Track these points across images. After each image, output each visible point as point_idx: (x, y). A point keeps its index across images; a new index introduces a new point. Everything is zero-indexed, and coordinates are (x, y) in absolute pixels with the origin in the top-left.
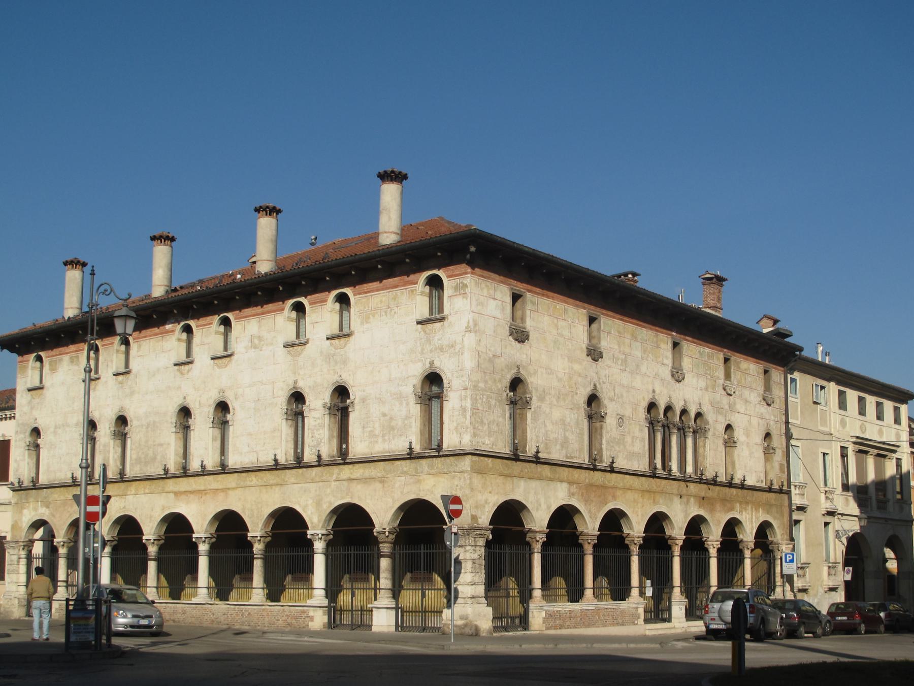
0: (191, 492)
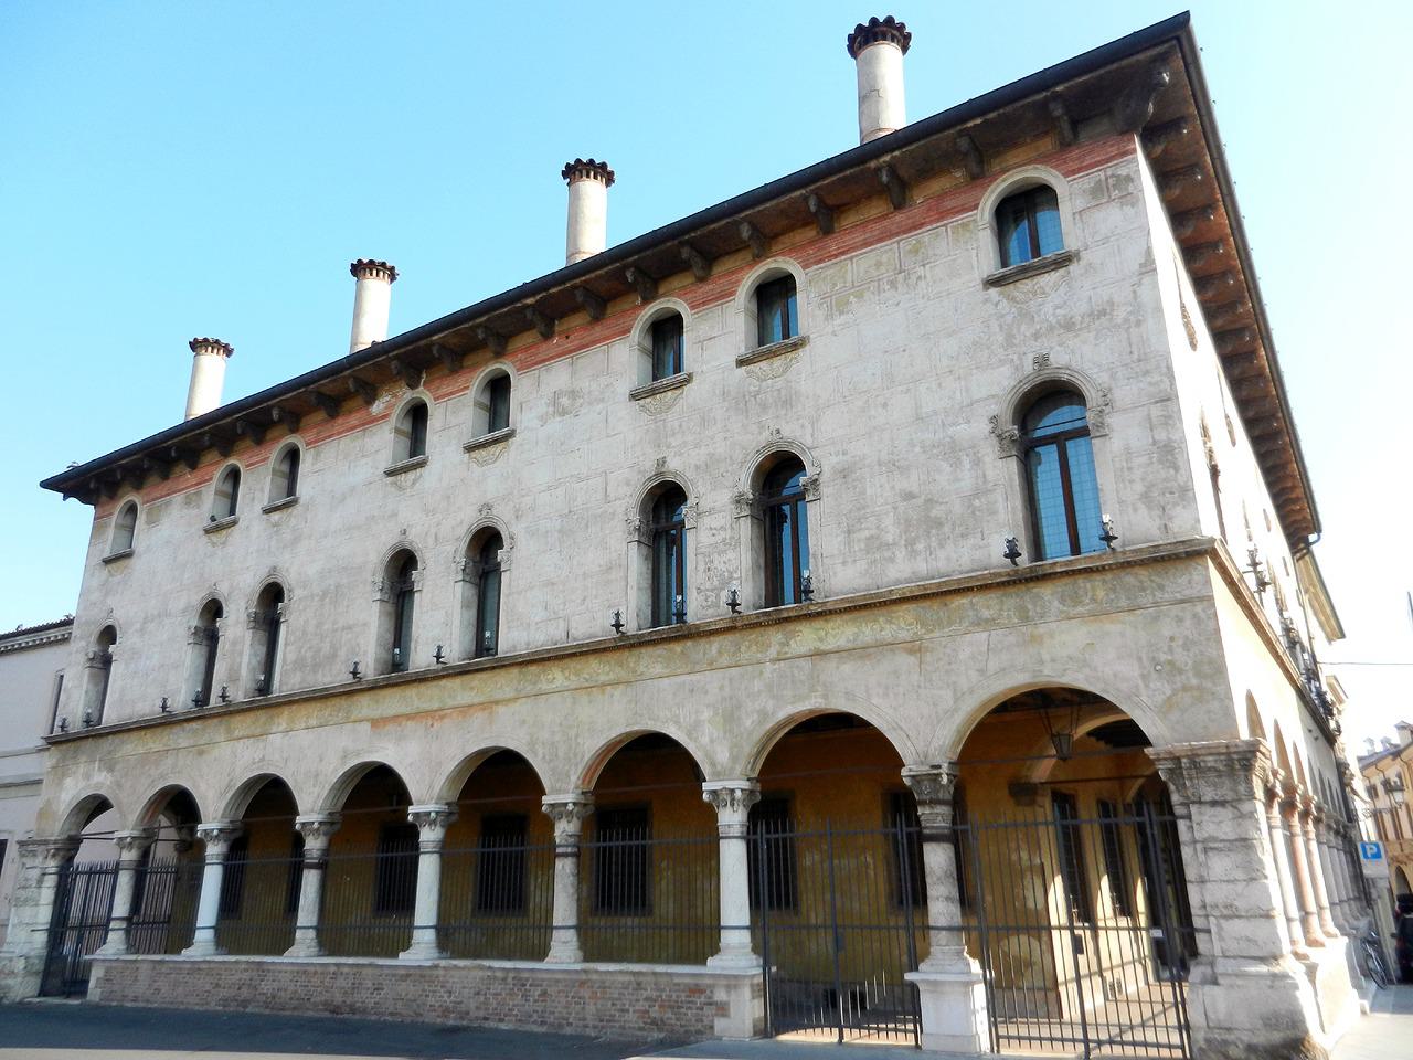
0: (409, 717)
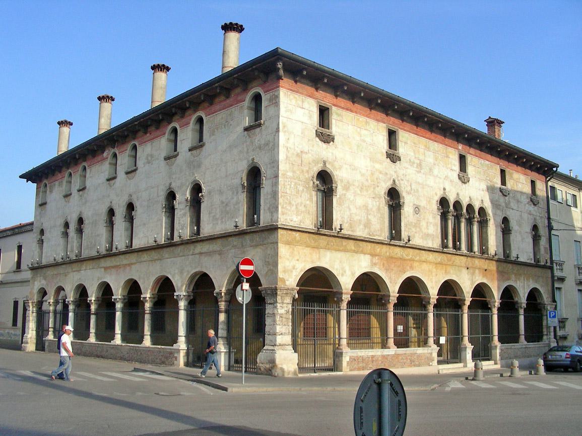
0: (113, 267)
